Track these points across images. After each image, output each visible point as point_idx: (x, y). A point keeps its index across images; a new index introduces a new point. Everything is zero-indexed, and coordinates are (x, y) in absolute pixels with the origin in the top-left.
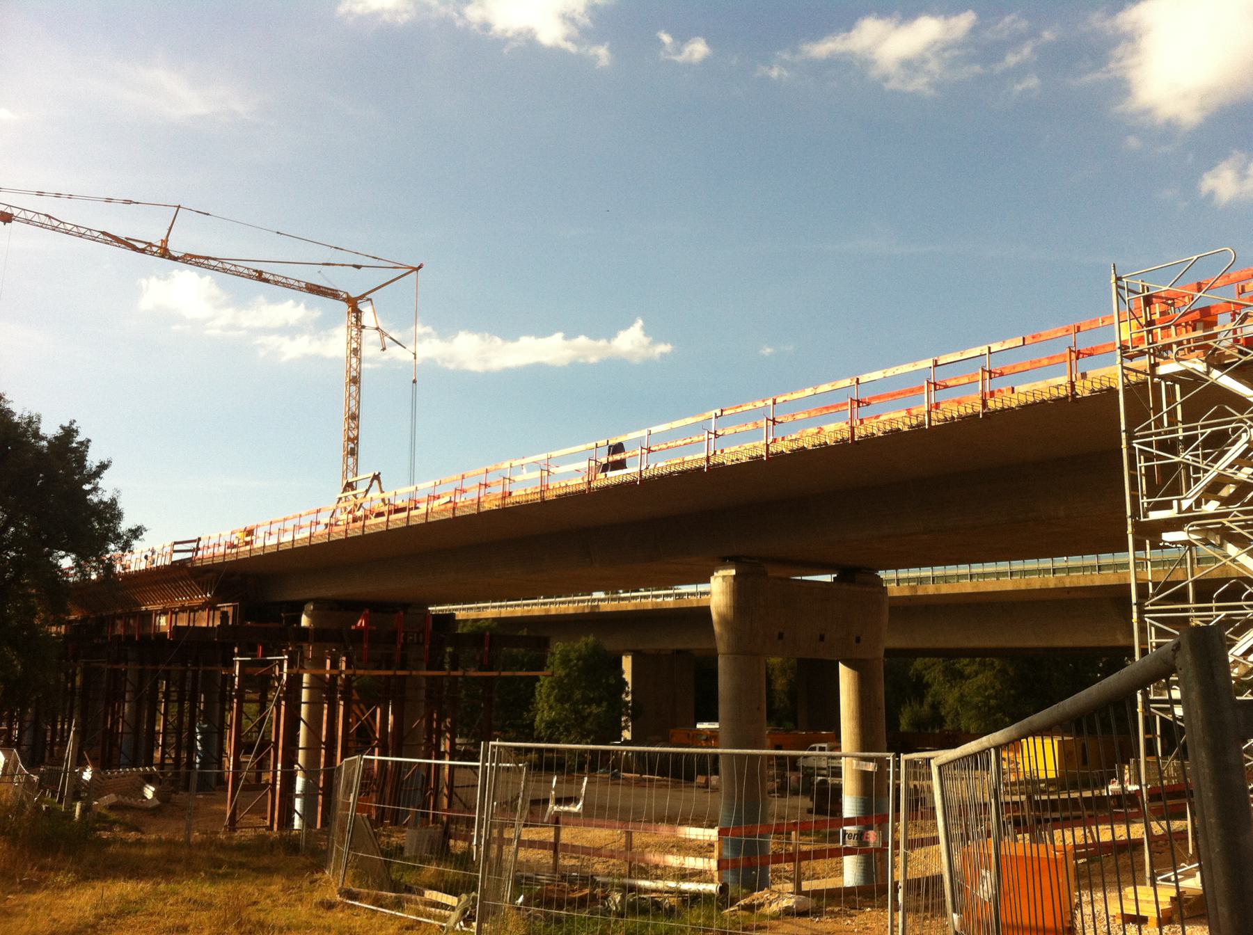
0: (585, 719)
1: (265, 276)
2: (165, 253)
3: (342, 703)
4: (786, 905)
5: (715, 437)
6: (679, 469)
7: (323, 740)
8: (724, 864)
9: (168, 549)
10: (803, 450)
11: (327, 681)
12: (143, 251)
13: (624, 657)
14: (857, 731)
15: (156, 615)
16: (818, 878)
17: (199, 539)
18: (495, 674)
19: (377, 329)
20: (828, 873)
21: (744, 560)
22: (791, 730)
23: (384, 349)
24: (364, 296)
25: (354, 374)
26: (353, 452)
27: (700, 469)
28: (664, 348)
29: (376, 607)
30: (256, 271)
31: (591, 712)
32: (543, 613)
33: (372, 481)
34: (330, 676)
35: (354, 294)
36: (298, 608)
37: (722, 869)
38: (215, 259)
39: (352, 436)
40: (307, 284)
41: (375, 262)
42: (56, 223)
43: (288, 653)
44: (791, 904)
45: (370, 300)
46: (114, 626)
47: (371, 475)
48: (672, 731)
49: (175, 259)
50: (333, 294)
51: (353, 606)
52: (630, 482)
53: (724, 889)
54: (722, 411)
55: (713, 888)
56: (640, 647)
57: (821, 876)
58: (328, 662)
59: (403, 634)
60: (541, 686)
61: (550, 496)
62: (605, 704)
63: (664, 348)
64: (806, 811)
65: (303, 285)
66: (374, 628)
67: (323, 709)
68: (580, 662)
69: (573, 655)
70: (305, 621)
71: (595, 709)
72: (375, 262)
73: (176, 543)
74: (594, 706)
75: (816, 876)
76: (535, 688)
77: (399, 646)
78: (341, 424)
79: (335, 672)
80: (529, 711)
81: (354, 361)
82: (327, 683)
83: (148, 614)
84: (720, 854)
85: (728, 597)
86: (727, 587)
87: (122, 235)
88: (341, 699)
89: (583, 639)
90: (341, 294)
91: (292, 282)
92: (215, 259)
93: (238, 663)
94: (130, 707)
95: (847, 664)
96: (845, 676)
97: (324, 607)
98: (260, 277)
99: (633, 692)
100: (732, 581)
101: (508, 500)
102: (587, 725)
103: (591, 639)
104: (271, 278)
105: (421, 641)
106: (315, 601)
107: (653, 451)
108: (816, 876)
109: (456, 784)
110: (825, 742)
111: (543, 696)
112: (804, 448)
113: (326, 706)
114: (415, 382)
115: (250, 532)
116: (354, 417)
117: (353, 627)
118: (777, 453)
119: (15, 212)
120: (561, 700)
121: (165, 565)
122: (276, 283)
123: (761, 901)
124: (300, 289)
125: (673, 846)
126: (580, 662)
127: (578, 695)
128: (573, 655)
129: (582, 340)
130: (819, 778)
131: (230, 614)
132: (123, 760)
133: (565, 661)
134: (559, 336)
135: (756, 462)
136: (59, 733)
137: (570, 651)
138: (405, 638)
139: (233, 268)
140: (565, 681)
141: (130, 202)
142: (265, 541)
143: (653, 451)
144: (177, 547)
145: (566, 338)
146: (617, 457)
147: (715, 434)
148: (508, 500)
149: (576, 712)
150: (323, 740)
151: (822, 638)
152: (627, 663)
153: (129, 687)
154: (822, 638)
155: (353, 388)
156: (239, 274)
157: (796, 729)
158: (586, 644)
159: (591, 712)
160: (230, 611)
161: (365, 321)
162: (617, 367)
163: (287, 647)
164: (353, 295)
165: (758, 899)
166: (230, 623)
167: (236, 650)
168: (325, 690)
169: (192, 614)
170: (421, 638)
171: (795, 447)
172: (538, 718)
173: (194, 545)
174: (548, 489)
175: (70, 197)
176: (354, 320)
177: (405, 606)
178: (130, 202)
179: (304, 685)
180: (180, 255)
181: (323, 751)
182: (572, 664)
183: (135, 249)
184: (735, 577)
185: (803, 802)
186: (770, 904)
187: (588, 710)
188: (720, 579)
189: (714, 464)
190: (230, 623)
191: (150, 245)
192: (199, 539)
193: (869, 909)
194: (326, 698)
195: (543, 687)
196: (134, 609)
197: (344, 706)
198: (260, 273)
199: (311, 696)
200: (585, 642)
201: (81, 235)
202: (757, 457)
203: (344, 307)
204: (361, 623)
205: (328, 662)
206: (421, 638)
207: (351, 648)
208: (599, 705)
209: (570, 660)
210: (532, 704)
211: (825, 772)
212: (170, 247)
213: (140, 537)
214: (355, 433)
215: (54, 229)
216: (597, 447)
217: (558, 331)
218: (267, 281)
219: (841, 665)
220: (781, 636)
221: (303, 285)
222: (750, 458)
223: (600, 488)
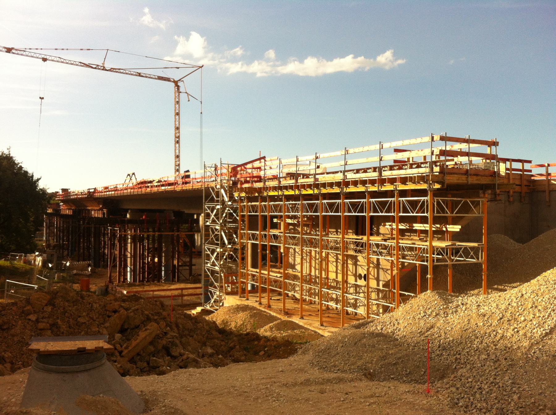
1: (142, 74)
2: (104, 69)
12: (95, 68)
19: (186, 93)
23: (189, 101)
25: (177, 111)
26: (178, 142)
28: (400, 62)
36: (126, 211)
38: (122, 69)
40: (158, 76)
41: (185, 66)
42: (62, 60)
49: (108, 70)
50: (168, 80)
51: (142, 211)
63: (400, 62)
70: (128, 216)
72: (185, 66)
78: (173, 131)
81: (177, 106)
83: (89, 210)
87: (87, 63)
92: (122, 69)
97: (134, 212)
98: (140, 75)
104: (144, 75)
106: (131, 209)
114: (201, 113)
119: (48, 57)
122: (146, 77)
124: (155, 79)
129: (361, 59)
134: (351, 56)
138: (160, 221)
139: (129, 73)
141: (89, 50)
145: (355, 57)
146: (187, 174)
156: (132, 74)
160: (105, 212)
161: (181, 90)
162: (378, 72)
164: (176, 80)
168: (134, 239)
175: (67, 49)
176: (176, 89)
178: (89, 50)
180: (109, 69)
183: (92, 68)
191: (98, 66)
198: (140, 74)
199: (131, 241)
201: (72, 64)
203: (173, 84)
212: (105, 66)
215: (62, 62)
217: (351, 54)
221: (157, 77)
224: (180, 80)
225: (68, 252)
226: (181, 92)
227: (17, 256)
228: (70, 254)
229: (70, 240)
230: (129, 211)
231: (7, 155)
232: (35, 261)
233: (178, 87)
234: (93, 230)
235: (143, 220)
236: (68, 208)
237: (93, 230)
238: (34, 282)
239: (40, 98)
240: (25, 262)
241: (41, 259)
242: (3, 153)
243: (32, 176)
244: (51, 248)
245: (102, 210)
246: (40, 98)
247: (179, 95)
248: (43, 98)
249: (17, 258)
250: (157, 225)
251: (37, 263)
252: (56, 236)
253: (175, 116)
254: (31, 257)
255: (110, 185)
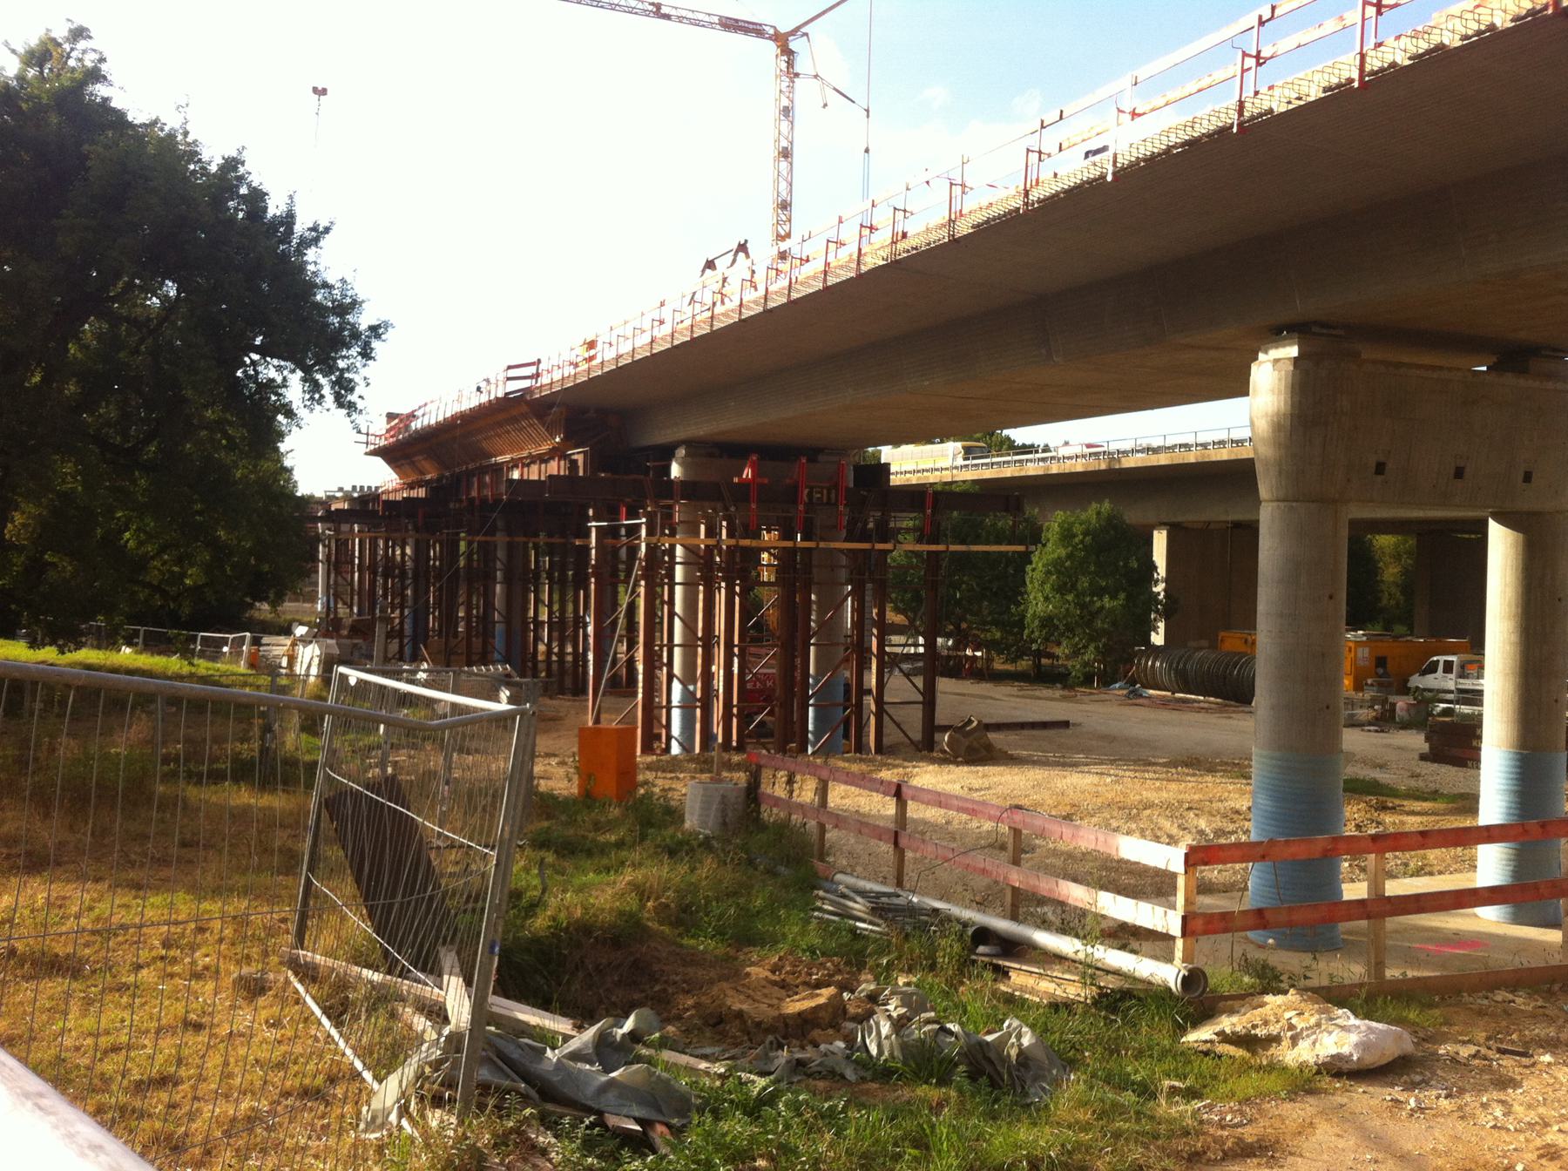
0: (1094, 615)
1: (664, 10)
3: (593, 580)
4: (1334, 1051)
5: (1259, 64)
6: (1184, 136)
7: (700, 635)
8: (1198, 924)
9: (501, 377)
10: (1439, 54)
11: (702, 554)
13: (1155, 533)
14: (1514, 638)
15: (508, 469)
16: (1431, 874)
17: (539, 361)
18: (941, 547)
20: (1449, 865)
21: (1315, 329)
22: (1401, 636)
24: (797, 29)
25: (784, 143)
27: (1223, 131)
29: (771, 452)
30: (652, 4)
31: (1102, 607)
32: (1041, 473)
33: (736, 254)
34: (706, 546)
35: (784, 28)
36: (667, 453)
37: (1193, 933)
39: (783, 233)
43: (647, 515)
44: (1346, 1050)
45: (806, 34)
46: (469, 487)
47: (735, 247)
48: (1222, 634)
50: (752, 29)
51: (732, 450)
52: (1095, 180)
53: (1193, 980)
54: (1273, 8)
55: (1167, 974)
56: (1180, 519)
57: (1436, 869)
58: (703, 527)
59: (806, 491)
60: (1033, 570)
61: (963, 228)
62: (1122, 596)
64: (1417, 757)
65: (716, 20)
66: (766, 481)
67: (698, 592)
68: (1088, 539)
69: (1078, 529)
70: (676, 471)
71: (1107, 602)
73: (510, 367)
74: (1106, 599)
75: (1427, 869)
76: (1024, 572)
77: (801, 507)
79: (711, 542)
80: (1018, 604)
82: (701, 557)
84: (1188, 902)
85: (1282, 398)
86: (1280, 380)
88: (723, 579)
89: (1094, 505)
90: (766, 28)
91: (701, 17)
93: (594, 530)
94: (502, 589)
95: (1503, 519)
96: (1501, 544)
97: (700, 450)
99: (1167, 580)
100: (1292, 368)
101: (901, 246)
102: (1098, 624)
103: (1106, 506)
104: (673, 12)
105: (833, 501)
106: (689, 443)
107: (1140, 115)
108: (1427, 869)
109: (886, 699)
110: (1454, 654)
111: (1036, 585)
112: (1441, 47)
113: (701, 588)
114: (867, 151)
115: (591, 345)
116: (785, 206)
117: (736, 480)
118: (1382, 70)
120: (1061, 589)
121: (497, 398)
122: (681, 19)
123: (1274, 1029)
125: (1189, 809)
126: (1088, 539)
127: (1084, 583)
128: (1078, 529)
130: (1443, 705)
131: (581, 463)
132: (496, 656)
133: (1067, 536)
135: (1339, 95)
136: (571, 624)
137: (1073, 523)
138: (810, 495)
140: (1068, 564)
142: (607, 356)
143: (1140, 115)
144: (512, 373)
147: (1258, 57)
148: (901, 246)
149: (1083, 606)
150: (700, 635)
151: (1459, 473)
152: (1160, 541)
153: (499, 565)
154: (1459, 473)
155: (784, 165)
157: (1411, 635)
158: (1098, 513)
159: (1102, 607)
160: (580, 458)
163: (644, 508)
164: (783, 29)
165: (1266, 1023)
166: (581, 474)
167: (591, 512)
168: (704, 569)
169: (543, 466)
170: (833, 496)
171: (1423, 46)
172: (1031, 611)
173: (532, 370)
174: (961, 215)
176: (784, 66)
177: (813, 452)
179: (678, 560)
181: (700, 650)
182: (1077, 540)
184: (1296, 361)
185: (1416, 741)
186: (1295, 1040)
187: (1098, 604)
188: (1270, 366)
189: (1253, 118)
190: (581, 474)
192: (539, 361)
193: (1547, 1058)
194: (701, 578)
195: (1036, 570)
196: (485, 463)
197: (646, 587)
199: (686, 574)
200: (1093, 512)
202: (1339, 86)
203: (771, 48)
204: (748, 473)
205: (703, 527)
206: (833, 496)
207: (733, 509)
208: (1113, 597)
209: (1074, 536)
210: (1022, 594)
211: (1450, 697)
213: (383, 337)
214: (787, 228)
216: (1042, 127)
218: (667, 17)
219: (1491, 521)
220: (1380, 468)
221: (716, 20)
222: (1325, 90)
223: (1044, 200)
224: (794, 32)
225: (402, 646)
226: (797, 75)
227: (225, 642)
228: (407, 650)
229: (410, 603)
230: (681, 452)
231: (171, 136)
232: (292, 660)
233: (788, 52)
234: (501, 554)
235: (745, 485)
236: (410, 480)
237: (501, 554)
238: (844, 560)
239: (315, 90)
240: (252, 665)
241: (317, 652)
242: (155, 122)
243: (289, 219)
244: (345, 632)
245: (563, 456)
246: (315, 90)
247: (791, 88)
248: (324, 92)
249: (225, 649)
250: (801, 507)
251: (299, 669)
252: (359, 594)
253: (777, 160)
254: (277, 647)
255: (773, 134)
